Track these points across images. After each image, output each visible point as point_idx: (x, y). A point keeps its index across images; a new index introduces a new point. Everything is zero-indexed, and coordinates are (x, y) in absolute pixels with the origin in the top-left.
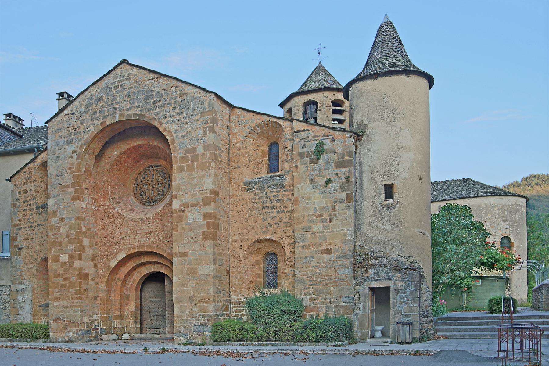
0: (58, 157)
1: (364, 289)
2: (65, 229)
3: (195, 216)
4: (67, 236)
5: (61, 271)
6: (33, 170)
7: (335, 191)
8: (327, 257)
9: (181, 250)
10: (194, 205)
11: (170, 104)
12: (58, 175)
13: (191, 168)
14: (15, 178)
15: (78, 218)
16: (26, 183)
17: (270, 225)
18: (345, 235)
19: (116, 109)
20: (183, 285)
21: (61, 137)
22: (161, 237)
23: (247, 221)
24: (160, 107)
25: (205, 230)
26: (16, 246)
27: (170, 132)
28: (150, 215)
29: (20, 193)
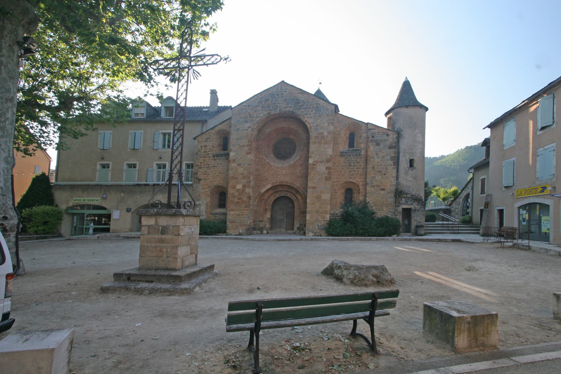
0: (238, 129)
1: (400, 209)
2: (241, 170)
3: (322, 168)
4: (242, 174)
5: (236, 194)
6: (212, 134)
7: (387, 160)
8: (382, 192)
9: (312, 185)
10: (321, 162)
11: (310, 108)
12: (237, 139)
13: (320, 143)
14: (199, 138)
15: (249, 165)
16: (206, 141)
17: (353, 175)
18: (392, 182)
19: (277, 106)
20: (313, 204)
21: (241, 118)
22: (293, 177)
23: (341, 172)
24: (303, 109)
25: (326, 175)
26: (197, 178)
27: (309, 122)
28: (286, 165)
29: (201, 147)
